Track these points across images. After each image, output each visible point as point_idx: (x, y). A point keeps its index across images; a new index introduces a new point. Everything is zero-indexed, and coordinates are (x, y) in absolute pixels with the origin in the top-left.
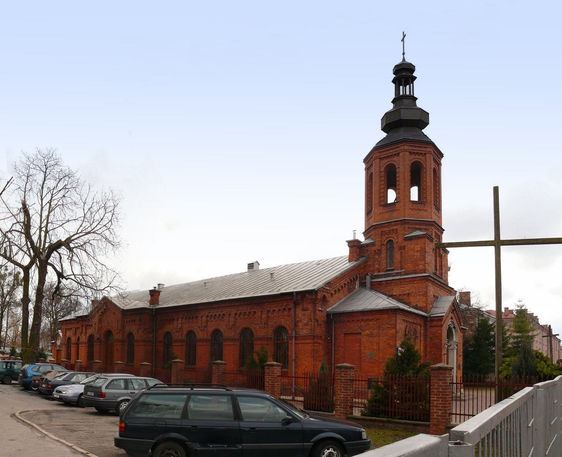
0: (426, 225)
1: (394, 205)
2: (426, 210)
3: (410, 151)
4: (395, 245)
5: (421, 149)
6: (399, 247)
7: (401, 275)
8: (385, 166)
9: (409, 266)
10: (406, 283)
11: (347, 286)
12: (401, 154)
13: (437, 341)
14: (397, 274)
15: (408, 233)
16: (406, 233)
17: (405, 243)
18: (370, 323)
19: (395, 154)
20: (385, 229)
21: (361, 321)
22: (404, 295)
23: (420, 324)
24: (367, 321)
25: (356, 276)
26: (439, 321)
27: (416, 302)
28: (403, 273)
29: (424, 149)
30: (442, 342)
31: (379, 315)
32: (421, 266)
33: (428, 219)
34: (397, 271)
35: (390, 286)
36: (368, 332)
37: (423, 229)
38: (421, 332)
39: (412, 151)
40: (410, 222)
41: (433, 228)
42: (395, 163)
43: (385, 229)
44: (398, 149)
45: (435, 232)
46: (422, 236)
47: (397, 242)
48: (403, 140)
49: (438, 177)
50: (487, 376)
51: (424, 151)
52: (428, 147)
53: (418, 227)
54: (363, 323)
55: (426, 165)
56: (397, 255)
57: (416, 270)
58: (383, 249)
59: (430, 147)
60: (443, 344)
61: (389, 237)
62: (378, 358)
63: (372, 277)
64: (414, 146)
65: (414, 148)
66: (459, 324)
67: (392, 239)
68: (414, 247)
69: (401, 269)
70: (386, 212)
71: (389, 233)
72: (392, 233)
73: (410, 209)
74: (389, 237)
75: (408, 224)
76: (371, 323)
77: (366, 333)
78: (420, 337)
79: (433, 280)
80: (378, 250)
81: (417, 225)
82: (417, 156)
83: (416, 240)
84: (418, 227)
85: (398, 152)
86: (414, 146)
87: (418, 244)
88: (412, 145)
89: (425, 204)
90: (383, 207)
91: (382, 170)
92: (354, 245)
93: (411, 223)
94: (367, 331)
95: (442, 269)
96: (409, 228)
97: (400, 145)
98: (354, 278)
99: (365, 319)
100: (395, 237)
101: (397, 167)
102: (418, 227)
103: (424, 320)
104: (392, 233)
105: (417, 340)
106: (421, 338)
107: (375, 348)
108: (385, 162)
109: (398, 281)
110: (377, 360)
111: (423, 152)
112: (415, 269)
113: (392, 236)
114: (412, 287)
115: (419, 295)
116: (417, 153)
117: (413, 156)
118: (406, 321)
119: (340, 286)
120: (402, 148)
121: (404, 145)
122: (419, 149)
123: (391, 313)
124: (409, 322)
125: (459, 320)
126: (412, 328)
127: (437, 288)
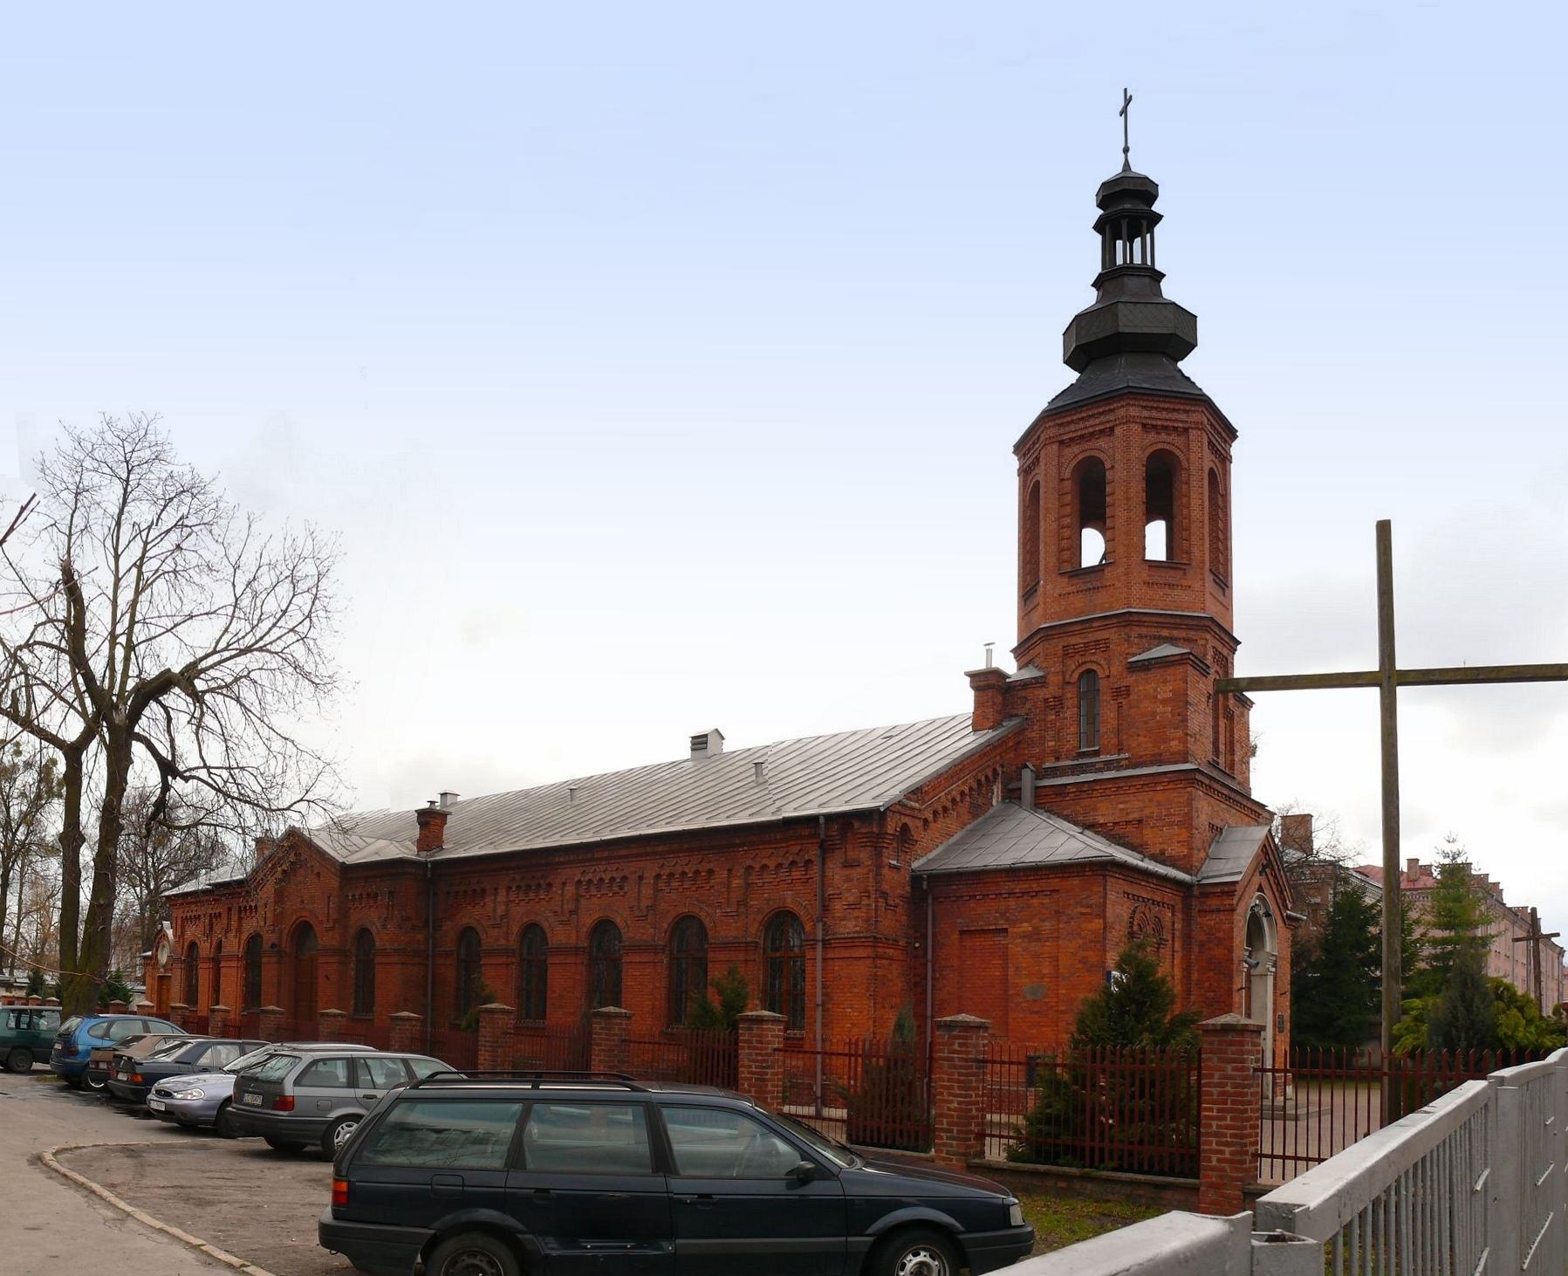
0: (1190, 627)
1: (1101, 573)
2: (1190, 587)
3: (1144, 421)
4: (1103, 685)
5: (1175, 416)
6: (1112, 689)
7: (1119, 768)
8: (1074, 463)
9: (1142, 744)
10: (1133, 790)
11: (968, 799)
12: (1118, 431)
13: (1219, 952)
14: (1108, 765)
15: (1138, 651)
16: (1134, 650)
17: (1131, 679)
18: (1031, 901)
19: (1102, 431)
20: (1073, 640)
21: (1007, 896)
22: (1127, 822)
23: (1172, 906)
26: (1224, 898)
27: (1160, 843)
28: (1123, 763)
29: (1183, 417)
30: (1234, 955)
31: (1056, 880)
32: (1173, 743)
33: (1194, 612)
34: (1109, 758)
35: (1089, 799)
36: (1026, 927)
37: (1180, 639)
38: (1173, 926)
39: (1149, 422)
40: (1144, 619)
41: (1208, 636)
42: (1102, 456)
43: (1073, 640)
44: (1111, 417)
45: (1214, 647)
46: (1177, 658)
47: (1108, 677)
48: (1126, 391)
49: (1222, 496)
51: (1182, 421)
52: (1195, 411)
53: (1165, 633)
54: (1012, 903)
55: (1188, 460)
56: (1108, 712)
57: (1161, 754)
58: (1069, 695)
59: (1198, 411)
60: (1236, 961)
61: (1085, 663)
62: (1056, 1000)
63: (1039, 775)
64: (1156, 408)
65: (1154, 414)
66: (1280, 905)
67: (1094, 667)
68: (1155, 690)
69: (1120, 751)
70: (1077, 592)
71: (1086, 651)
72: (1094, 651)
73: (1144, 583)
74: (1085, 663)
75: (1137, 626)
76: (1035, 901)
77: (1020, 930)
78: (1173, 941)
79: (1207, 782)
80: (1055, 698)
81: (1164, 627)
82: (1163, 436)
83: (1161, 670)
84: (1165, 633)
85: (1111, 424)
86: (1156, 408)
87: (1165, 682)
88: (1150, 404)
89: (1185, 569)
90: (1070, 577)
91: (1067, 474)
92: (987, 683)
93: (1146, 624)
94: (1025, 925)
95: (1232, 752)
96: (1140, 636)
97: (1115, 405)
98: (987, 777)
99: (1017, 891)
100: (1103, 662)
101: (1108, 465)
102: (1167, 634)
103: (1182, 894)
105: (1163, 950)
106: (1174, 944)
107: (1045, 971)
108: (1075, 453)
109: (1111, 786)
110: (1053, 1004)
111: (1180, 425)
112: (1156, 751)
113: (1092, 659)
114: (1151, 801)
115: (1170, 824)
116: (1162, 426)
117: (1152, 436)
118: (1134, 895)
119: (949, 797)
121: (1128, 405)
122: (1170, 416)
123: (1090, 873)
124: (1141, 899)
125: (1281, 893)
126: (1148, 917)
127: (1219, 805)
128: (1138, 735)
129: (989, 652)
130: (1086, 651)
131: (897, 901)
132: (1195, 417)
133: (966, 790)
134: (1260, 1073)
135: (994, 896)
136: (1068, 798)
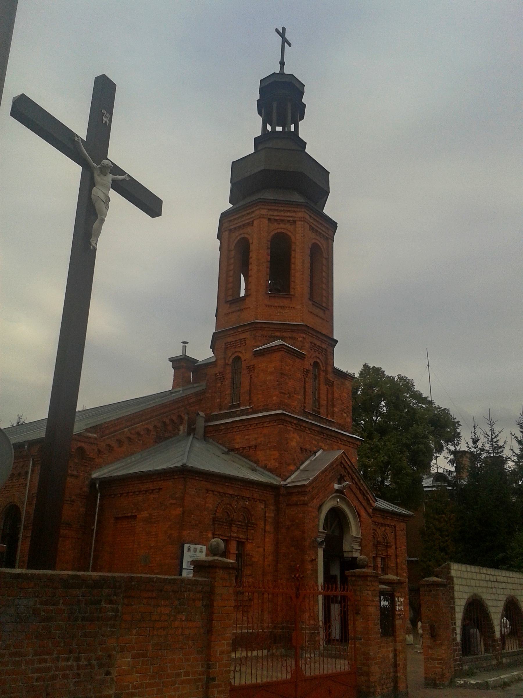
2: (294, 308)
3: (269, 217)
5: (288, 214)
6: (247, 367)
7: (247, 414)
12: (255, 223)
15: (260, 344)
16: (259, 344)
22: (250, 447)
24: (147, 494)
25: (180, 416)
29: (294, 214)
31: (161, 482)
33: (297, 322)
34: (245, 408)
35: (231, 433)
36: (145, 514)
37: (287, 337)
38: (265, 514)
39: (273, 217)
40: (264, 326)
44: (253, 215)
45: (311, 343)
46: (276, 348)
48: (259, 200)
50: (161, 654)
51: (292, 217)
52: (299, 211)
53: (278, 334)
55: (295, 238)
57: (268, 405)
58: (228, 371)
59: (301, 211)
61: (236, 352)
63: (209, 418)
64: (277, 210)
67: (240, 355)
70: (271, 306)
71: (231, 347)
72: (239, 345)
73: (266, 306)
74: (236, 352)
80: (220, 373)
82: (282, 225)
84: (278, 334)
85: (251, 220)
86: (277, 210)
88: (273, 208)
89: (291, 298)
90: (230, 304)
91: (232, 247)
94: (146, 512)
96: (263, 336)
99: (143, 489)
100: (243, 352)
102: (279, 335)
103: (274, 493)
104: (239, 345)
109: (241, 425)
111: (291, 219)
116: (281, 220)
117: (275, 225)
120: (257, 213)
121: (261, 208)
122: (285, 214)
125: (364, 495)
128: (258, 394)
129: (185, 348)
130: (231, 347)
131: (73, 497)
132: (300, 215)
133: (151, 427)
134: (148, 629)
135: (132, 494)
136: (221, 433)
